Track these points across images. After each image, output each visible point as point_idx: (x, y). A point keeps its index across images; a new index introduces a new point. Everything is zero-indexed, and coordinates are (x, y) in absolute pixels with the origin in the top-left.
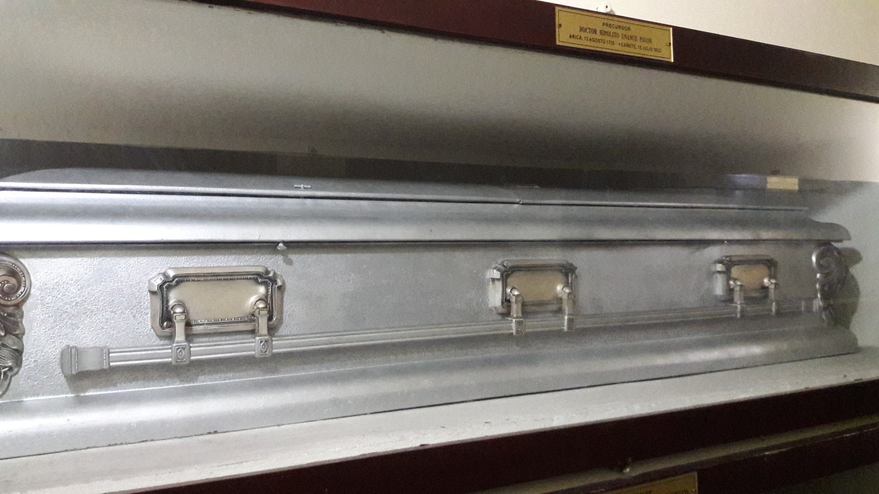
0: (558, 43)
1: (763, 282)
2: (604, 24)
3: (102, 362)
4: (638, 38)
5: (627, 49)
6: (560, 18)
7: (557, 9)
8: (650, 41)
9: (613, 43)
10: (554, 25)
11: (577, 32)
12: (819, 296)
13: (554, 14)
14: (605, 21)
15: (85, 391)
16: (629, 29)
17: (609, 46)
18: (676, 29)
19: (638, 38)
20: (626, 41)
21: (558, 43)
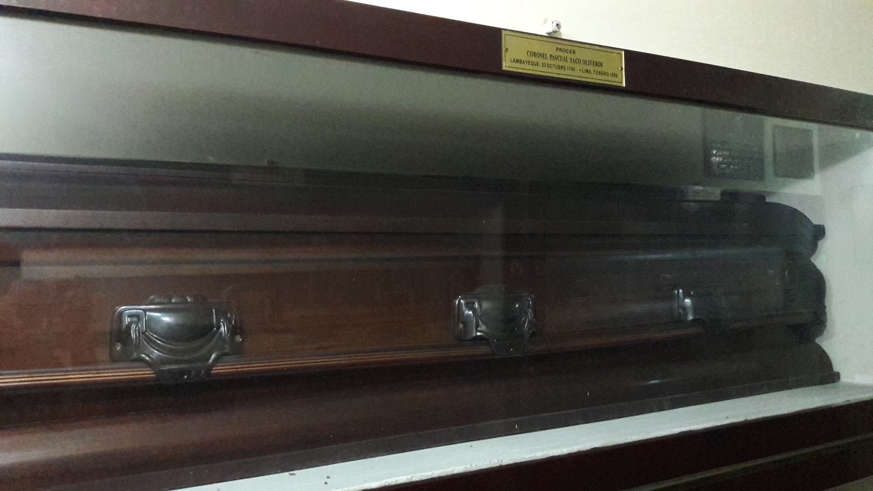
0: (504, 68)
1: (242, 337)
2: (557, 49)
3: (112, 326)
4: (548, 56)
5: (562, 71)
6: (507, 42)
7: (504, 32)
8: (601, 64)
9: (573, 69)
10: (501, 49)
11: (524, 57)
12: (478, 334)
13: (501, 38)
14: (559, 46)
15: (132, 340)
16: (574, 52)
17: (570, 72)
18: (628, 53)
19: (548, 56)
20: (586, 67)
21: (504, 68)
